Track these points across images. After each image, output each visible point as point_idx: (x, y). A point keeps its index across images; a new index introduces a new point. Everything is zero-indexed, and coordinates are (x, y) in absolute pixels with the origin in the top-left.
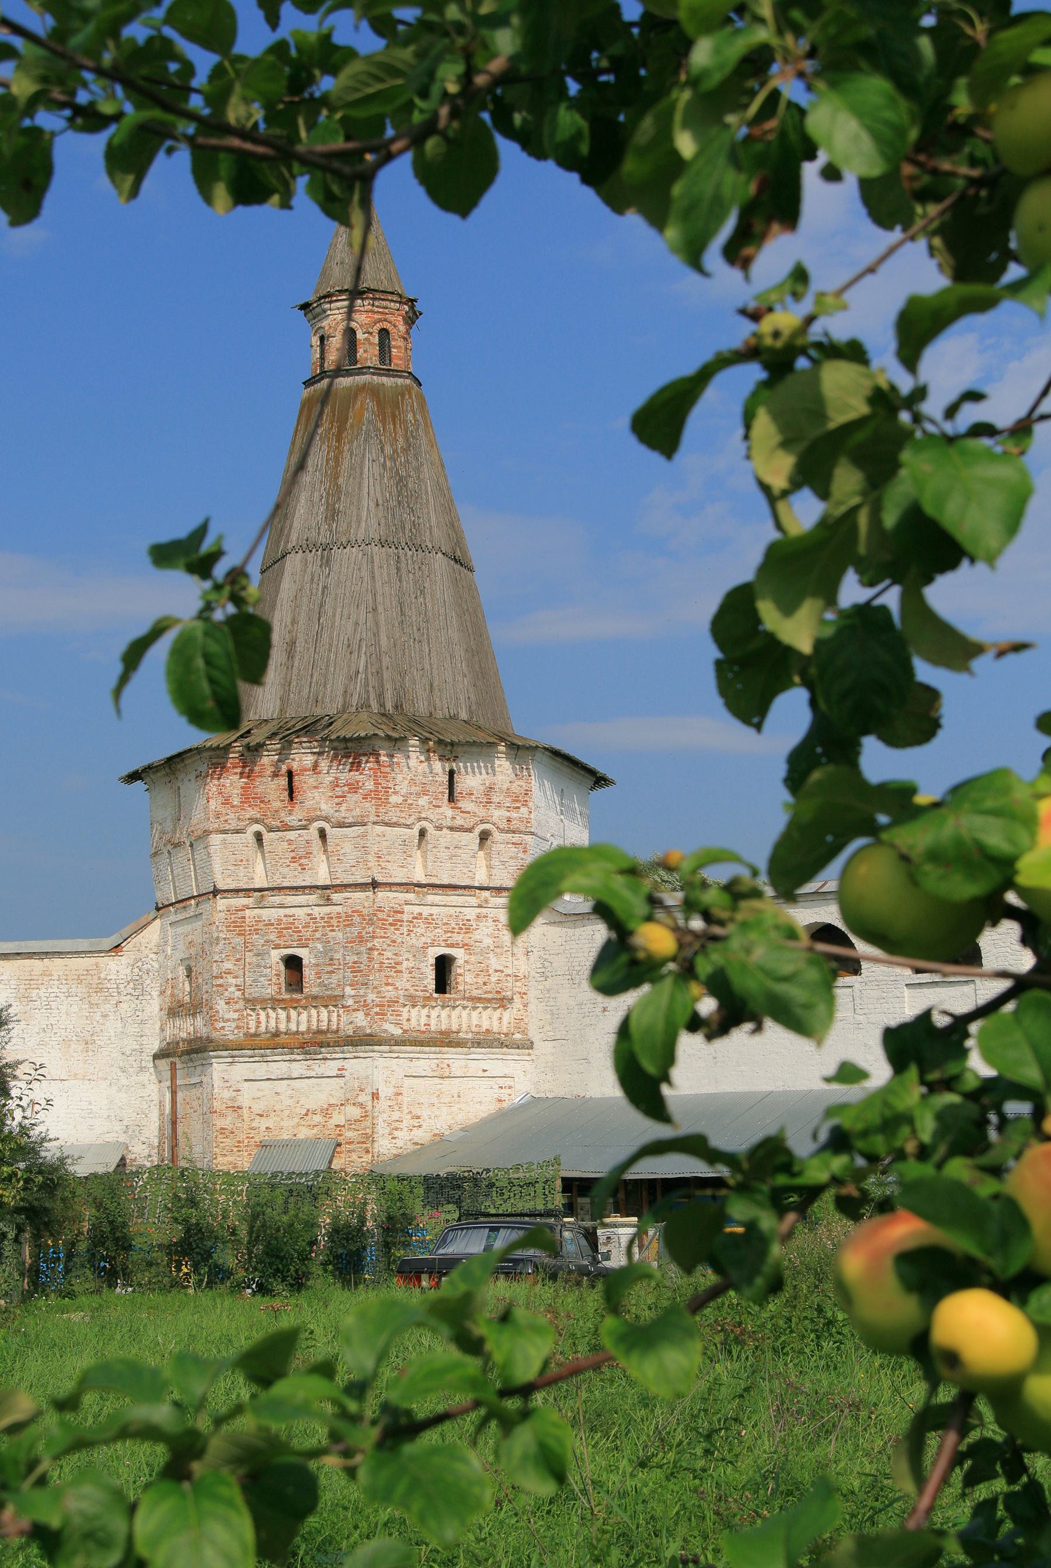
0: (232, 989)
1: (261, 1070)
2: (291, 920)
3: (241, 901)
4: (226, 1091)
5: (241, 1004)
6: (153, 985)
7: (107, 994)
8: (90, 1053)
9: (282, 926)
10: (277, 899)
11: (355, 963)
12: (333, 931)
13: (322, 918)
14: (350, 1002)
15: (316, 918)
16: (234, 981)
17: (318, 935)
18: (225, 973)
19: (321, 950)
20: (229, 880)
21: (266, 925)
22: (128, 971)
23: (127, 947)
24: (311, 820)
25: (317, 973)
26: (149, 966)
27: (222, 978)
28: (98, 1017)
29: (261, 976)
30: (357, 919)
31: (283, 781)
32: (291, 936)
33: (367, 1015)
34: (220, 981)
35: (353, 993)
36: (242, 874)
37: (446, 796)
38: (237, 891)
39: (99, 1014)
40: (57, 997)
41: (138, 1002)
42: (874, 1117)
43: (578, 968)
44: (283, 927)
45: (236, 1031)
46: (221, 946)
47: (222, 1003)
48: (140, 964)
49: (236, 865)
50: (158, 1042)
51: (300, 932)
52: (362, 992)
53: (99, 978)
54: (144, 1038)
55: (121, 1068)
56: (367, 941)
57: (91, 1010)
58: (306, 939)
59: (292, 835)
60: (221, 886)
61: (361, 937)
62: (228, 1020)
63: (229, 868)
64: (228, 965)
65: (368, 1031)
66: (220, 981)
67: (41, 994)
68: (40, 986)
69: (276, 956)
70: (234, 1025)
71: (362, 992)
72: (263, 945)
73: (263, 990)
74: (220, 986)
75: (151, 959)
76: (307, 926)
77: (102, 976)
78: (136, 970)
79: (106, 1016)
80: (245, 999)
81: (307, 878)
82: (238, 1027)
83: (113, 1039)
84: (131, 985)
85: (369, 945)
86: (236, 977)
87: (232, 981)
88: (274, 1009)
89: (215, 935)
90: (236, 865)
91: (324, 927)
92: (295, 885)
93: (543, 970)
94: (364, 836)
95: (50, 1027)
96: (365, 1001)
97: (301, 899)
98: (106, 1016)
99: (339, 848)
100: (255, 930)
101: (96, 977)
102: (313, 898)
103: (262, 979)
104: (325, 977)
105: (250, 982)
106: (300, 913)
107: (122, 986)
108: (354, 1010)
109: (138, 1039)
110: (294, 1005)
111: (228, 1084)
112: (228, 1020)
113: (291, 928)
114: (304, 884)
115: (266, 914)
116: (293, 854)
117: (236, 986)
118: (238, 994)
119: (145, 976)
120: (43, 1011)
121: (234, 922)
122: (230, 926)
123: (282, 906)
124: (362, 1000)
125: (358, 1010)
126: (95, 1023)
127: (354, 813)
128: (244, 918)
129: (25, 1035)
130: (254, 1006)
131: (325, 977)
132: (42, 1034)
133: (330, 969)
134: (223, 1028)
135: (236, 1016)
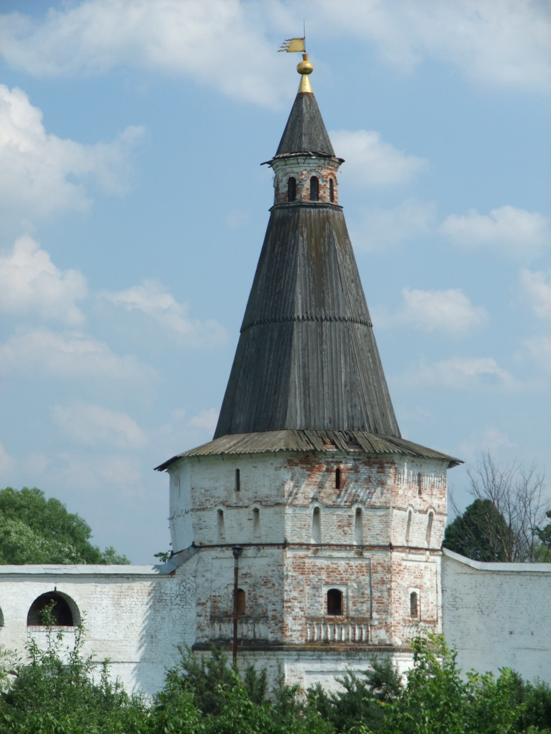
0: (297, 610)
1: (317, 666)
2: (335, 566)
3: (302, 553)
4: (293, 678)
5: (304, 620)
6: (192, 598)
7: (164, 604)
8: (154, 644)
9: (330, 570)
10: (327, 553)
11: (379, 597)
12: (363, 575)
13: (357, 567)
14: (376, 623)
15: (352, 566)
16: (299, 605)
17: (353, 577)
18: (293, 599)
19: (356, 587)
20: (295, 538)
21: (319, 569)
22: (177, 588)
23: (178, 571)
24: (353, 502)
25: (353, 603)
26: (190, 586)
27: (290, 602)
28: (159, 619)
29: (316, 602)
30: (379, 568)
31: (334, 475)
32: (336, 577)
33: (387, 631)
34: (289, 604)
35: (378, 617)
36: (304, 534)
37: (417, 491)
38: (301, 545)
39: (160, 617)
40: (136, 604)
41: (183, 610)
42: (362, 662)
43: (487, 605)
44: (330, 572)
45: (300, 638)
46: (289, 581)
47: (290, 619)
48: (184, 584)
49: (301, 528)
50: (194, 638)
51: (342, 574)
52: (384, 617)
53: (161, 592)
54: (186, 635)
55: (171, 655)
56: (387, 583)
57: (155, 615)
58: (346, 580)
59: (340, 512)
60: (290, 540)
61: (383, 581)
62: (294, 631)
63: (296, 529)
64: (295, 594)
65: (388, 643)
66: (289, 604)
67: (127, 603)
68: (126, 597)
69: (325, 590)
70: (299, 634)
71: (384, 617)
72: (317, 582)
73: (317, 612)
74: (289, 607)
75: (192, 581)
76: (346, 571)
77: (162, 591)
78: (182, 588)
79: (164, 618)
80: (306, 617)
81: (347, 540)
82: (301, 636)
83: (167, 634)
84: (179, 598)
85: (388, 586)
86: (300, 602)
87: (296, 603)
88: (324, 624)
89: (285, 573)
90: (301, 528)
91: (357, 572)
92: (339, 543)
93: (454, 603)
94: (386, 515)
95: (131, 625)
96: (386, 623)
97: (343, 554)
98: (164, 618)
99: (370, 522)
100: (312, 571)
101: (158, 592)
102: (352, 554)
103: (316, 604)
104: (359, 605)
105: (308, 606)
106: (343, 563)
107: (173, 598)
108: (378, 628)
109: (183, 635)
110: (334, 623)
111: (295, 674)
112: (294, 631)
113: (335, 572)
114: (345, 543)
115: (320, 562)
116: (339, 524)
117: (300, 608)
118: (302, 613)
119: (187, 593)
120: (128, 614)
121: (298, 565)
122: (295, 568)
123: (331, 557)
124: (384, 622)
125: (381, 628)
126: (157, 623)
127: (381, 500)
128: (304, 563)
129: (117, 631)
130: (312, 622)
131: (359, 605)
132: (127, 630)
133: (362, 600)
134: (291, 636)
135: (300, 628)
